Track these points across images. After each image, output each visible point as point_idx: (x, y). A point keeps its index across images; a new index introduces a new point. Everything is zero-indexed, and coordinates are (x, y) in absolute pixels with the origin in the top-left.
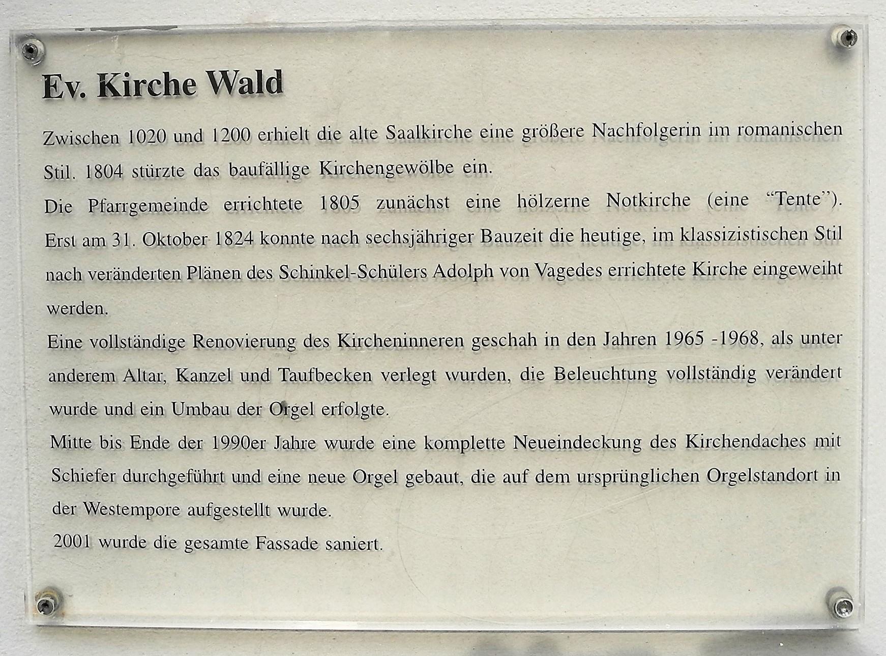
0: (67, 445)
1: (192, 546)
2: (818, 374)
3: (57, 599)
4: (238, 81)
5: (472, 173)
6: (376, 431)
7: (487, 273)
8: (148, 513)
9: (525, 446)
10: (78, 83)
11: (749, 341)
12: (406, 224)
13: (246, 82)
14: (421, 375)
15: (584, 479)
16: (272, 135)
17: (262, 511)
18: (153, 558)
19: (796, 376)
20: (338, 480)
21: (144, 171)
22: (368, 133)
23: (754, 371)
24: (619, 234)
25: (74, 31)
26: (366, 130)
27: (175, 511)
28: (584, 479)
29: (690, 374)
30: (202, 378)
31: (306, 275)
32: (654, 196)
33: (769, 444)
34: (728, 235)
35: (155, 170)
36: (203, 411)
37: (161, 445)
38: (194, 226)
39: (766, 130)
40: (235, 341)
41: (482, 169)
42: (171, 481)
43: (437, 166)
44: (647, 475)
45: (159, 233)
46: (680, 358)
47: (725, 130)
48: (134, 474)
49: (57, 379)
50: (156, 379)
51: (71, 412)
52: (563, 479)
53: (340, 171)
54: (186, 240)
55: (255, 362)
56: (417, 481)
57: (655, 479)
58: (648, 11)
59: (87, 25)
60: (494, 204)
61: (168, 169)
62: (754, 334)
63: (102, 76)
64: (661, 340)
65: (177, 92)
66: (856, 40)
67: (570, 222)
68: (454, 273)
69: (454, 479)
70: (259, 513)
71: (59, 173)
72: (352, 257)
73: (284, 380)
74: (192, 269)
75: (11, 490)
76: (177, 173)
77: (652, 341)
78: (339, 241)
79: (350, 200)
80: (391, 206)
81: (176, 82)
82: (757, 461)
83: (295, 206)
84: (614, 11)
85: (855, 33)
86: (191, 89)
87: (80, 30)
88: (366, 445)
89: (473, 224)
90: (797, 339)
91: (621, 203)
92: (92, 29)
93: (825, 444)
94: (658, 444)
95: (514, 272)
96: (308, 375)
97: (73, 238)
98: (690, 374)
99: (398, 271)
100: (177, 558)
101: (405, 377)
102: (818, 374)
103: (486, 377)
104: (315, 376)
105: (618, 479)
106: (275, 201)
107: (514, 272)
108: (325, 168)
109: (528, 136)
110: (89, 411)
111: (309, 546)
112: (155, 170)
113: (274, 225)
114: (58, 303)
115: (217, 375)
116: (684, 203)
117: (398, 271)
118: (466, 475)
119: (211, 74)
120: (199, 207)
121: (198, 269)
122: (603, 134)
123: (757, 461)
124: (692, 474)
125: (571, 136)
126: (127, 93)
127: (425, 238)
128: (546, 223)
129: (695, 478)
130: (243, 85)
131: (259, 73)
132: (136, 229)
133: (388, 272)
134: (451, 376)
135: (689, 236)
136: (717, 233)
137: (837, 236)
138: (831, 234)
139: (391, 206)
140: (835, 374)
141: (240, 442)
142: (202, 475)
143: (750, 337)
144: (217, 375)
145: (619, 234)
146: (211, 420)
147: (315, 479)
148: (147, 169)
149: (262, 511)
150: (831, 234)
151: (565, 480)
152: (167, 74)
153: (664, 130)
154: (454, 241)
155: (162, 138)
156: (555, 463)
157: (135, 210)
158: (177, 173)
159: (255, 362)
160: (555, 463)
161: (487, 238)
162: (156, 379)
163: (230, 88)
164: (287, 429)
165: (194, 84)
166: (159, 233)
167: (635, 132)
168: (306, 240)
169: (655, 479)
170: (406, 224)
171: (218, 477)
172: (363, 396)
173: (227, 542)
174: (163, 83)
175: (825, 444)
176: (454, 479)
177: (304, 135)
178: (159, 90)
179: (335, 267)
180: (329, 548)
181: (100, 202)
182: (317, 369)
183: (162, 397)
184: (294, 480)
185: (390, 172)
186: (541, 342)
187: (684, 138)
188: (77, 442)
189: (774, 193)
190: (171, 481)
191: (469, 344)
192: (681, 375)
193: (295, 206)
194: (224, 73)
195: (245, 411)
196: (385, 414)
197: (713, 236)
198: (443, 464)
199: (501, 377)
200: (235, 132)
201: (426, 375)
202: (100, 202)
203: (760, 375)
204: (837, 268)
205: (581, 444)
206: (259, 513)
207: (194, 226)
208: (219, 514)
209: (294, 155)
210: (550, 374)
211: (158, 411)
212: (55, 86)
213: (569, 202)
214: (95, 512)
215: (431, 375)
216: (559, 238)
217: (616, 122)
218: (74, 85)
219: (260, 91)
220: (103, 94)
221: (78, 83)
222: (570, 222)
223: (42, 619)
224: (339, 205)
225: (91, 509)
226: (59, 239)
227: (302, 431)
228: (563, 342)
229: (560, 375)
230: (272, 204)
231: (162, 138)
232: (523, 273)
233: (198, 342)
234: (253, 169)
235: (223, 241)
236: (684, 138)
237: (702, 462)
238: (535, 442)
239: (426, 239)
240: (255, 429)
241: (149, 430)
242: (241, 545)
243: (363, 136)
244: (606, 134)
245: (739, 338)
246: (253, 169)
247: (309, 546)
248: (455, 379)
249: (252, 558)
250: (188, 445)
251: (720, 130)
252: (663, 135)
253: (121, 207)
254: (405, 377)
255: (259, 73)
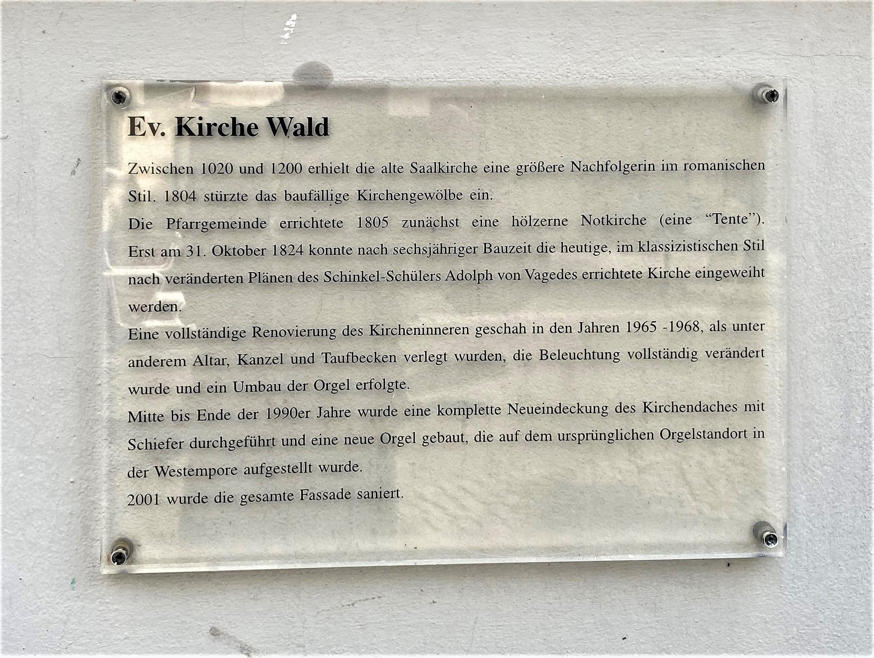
0: (143, 420)
1: (247, 500)
2: (747, 354)
3: (129, 550)
4: (292, 125)
5: (219, 448)
6: (397, 401)
7: (488, 276)
8: (211, 473)
9: (516, 412)
10: (159, 124)
11: (692, 329)
12: (424, 239)
13: (299, 126)
14: (436, 356)
15: (564, 438)
16: (320, 170)
17: (306, 468)
18: (214, 511)
19: (730, 355)
20: (368, 441)
21: (214, 196)
22: (396, 168)
23: (696, 352)
24: (590, 246)
25: (155, 82)
26: (394, 166)
27: (233, 471)
28: (564, 438)
29: (646, 355)
30: (258, 362)
31: (345, 279)
32: (618, 217)
33: (708, 409)
34: (682, 248)
35: (223, 196)
36: (258, 388)
37: (223, 416)
38: (256, 240)
39: (705, 166)
40: (287, 332)
41: (485, 196)
42: (231, 446)
43: (450, 194)
44: (612, 434)
45: (226, 246)
46: (638, 342)
47: (674, 167)
48: (199, 442)
49: (137, 364)
50: (221, 363)
51: (147, 391)
52: (546, 437)
53: (373, 198)
54: (248, 252)
55: (302, 349)
56: (432, 441)
57: (619, 438)
58: (614, 73)
59: (167, 78)
60: (493, 224)
61: (234, 195)
62: (696, 323)
63: (180, 119)
64: (624, 328)
65: (242, 134)
66: (778, 97)
67: (551, 237)
68: (462, 277)
69: (461, 439)
70: (303, 470)
71: (142, 197)
72: (382, 266)
73: (326, 362)
74: (253, 275)
75: (90, 457)
76: (241, 198)
77: (616, 329)
78: (372, 252)
79: (381, 220)
80: (413, 225)
81: (242, 125)
82: (699, 422)
83: (337, 225)
84: (588, 73)
85: (777, 92)
86: (254, 131)
87: (161, 81)
88: (390, 412)
89: (479, 240)
90: (729, 327)
91: (592, 222)
92: (171, 81)
93: (752, 409)
94: (622, 409)
95: (509, 276)
96: (346, 358)
97: (152, 249)
98: (646, 355)
99: (418, 275)
100: (232, 511)
101: (423, 358)
102: (747, 354)
103: (486, 358)
104: (351, 359)
105: (590, 437)
106: (321, 221)
107: (509, 276)
108: (362, 195)
109: (521, 171)
110: (163, 390)
111: (345, 496)
112: (223, 196)
113: (320, 240)
114: (138, 302)
115: (272, 359)
116: (641, 222)
117: (418, 275)
118: (469, 437)
119: (270, 120)
120: (259, 225)
121: (258, 274)
122: (579, 169)
123: (699, 422)
124: (648, 433)
125: (554, 171)
126: (201, 134)
127: (439, 250)
128: (533, 238)
129: (650, 436)
130: (296, 129)
131: (310, 119)
132: (207, 243)
133: (410, 276)
134: (459, 357)
135: (645, 248)
136: (667, 246)
137: (761, 247)
138: (756, 246)
139: (413, 225)
140: (760, 354)
141: (289, 413)
142: (257, 441)
143: (693, 326)
144: (272, 359)
145: (590, 246)
146: (263, 397)
147: (350, 441)
148: (217, 195)
149: (306, 468)
150: (756, 246)
151: (548, 438)
152: (234, 119)
153: (626, 166)
154: (462, 252)
155: (229, 170)
156: (541, 424)
157: (207, 227)
158: (241, 198)
159: (302, 349)
160: (541, 424)
161: (488, 250)
162: (221, 362)
163: (286, 131)
164: (328, 402)
165: (256, 127)
166: (226, 246)
167: (604, 168)
168: (342, 252)
169: (619, 438)
170: (424, 239)
171: (270, 442)
172: (389, 374)
173: (276, 495)
174: (231, 125)
175: (752, 409)
176: (461, 439)
177: (345, 169)
178: (228, 131)
179: (368, 273)
180: (360, 497)
181: (176, 220)
182: (353, 353)
183: (225, 378)
184: (333, 442)
185: (413, 199)
186: (529, 330)
187: (642, 172)
188: (152, 417)
189: (711, 215)
190: (231, 446)
191: (473, 332)
192: (639, 355)
193: (337, 225)
194: (281, 119)
195: (295, 387)
196: (406, 388)
197: (664, 247)
198: (451, 426)
199: (498, 357)
200: (290, 166)
201: (439, 357)
202: (176, 220)
203: (701, 355)
204: (761, 272)
205: (561, 410)
206: (303, 470)
207: (256, 240)
208: (270, 472)
209: (338, 186)
210: (536, 355)
211: (222, 389)
212: (139, 126)
213: (552, 222)
214: (165, 474)
215: (443, 357)
216: (544, 249)
217: (590, 161)
218: (155, 126)
219: (310, 134)
220: (180, 133)
221: (159, 124)
222: (551, 237)
223: (114, 568)
224: (372, 224)
225: (162, 472)
226: (140, 251)
227: (341, 402)
228: (547, 330)
229: (544, 355)
230: (319, 223)
231: (229, 170)
232: (516, 277)
233: (257, 332)
234: (304, 196)
235: (278, 252)
236: (642, 172)
237: (656, 424)
238: (525, 409)
239: (441, 251)
240: (301, 402)
241: (213, 405)
242: (289, 497)
243: (392, 170)
244: (581, 170)
245: (684, 326)
246: (304, 196)
247: (345, 496)
248: (462, 360)
249: (295, 510)
250: (245, 416)
251: (670, 166)
252: (625, 170)
253: (194, 225)
254: (423, 358)
255: (310, 119)
